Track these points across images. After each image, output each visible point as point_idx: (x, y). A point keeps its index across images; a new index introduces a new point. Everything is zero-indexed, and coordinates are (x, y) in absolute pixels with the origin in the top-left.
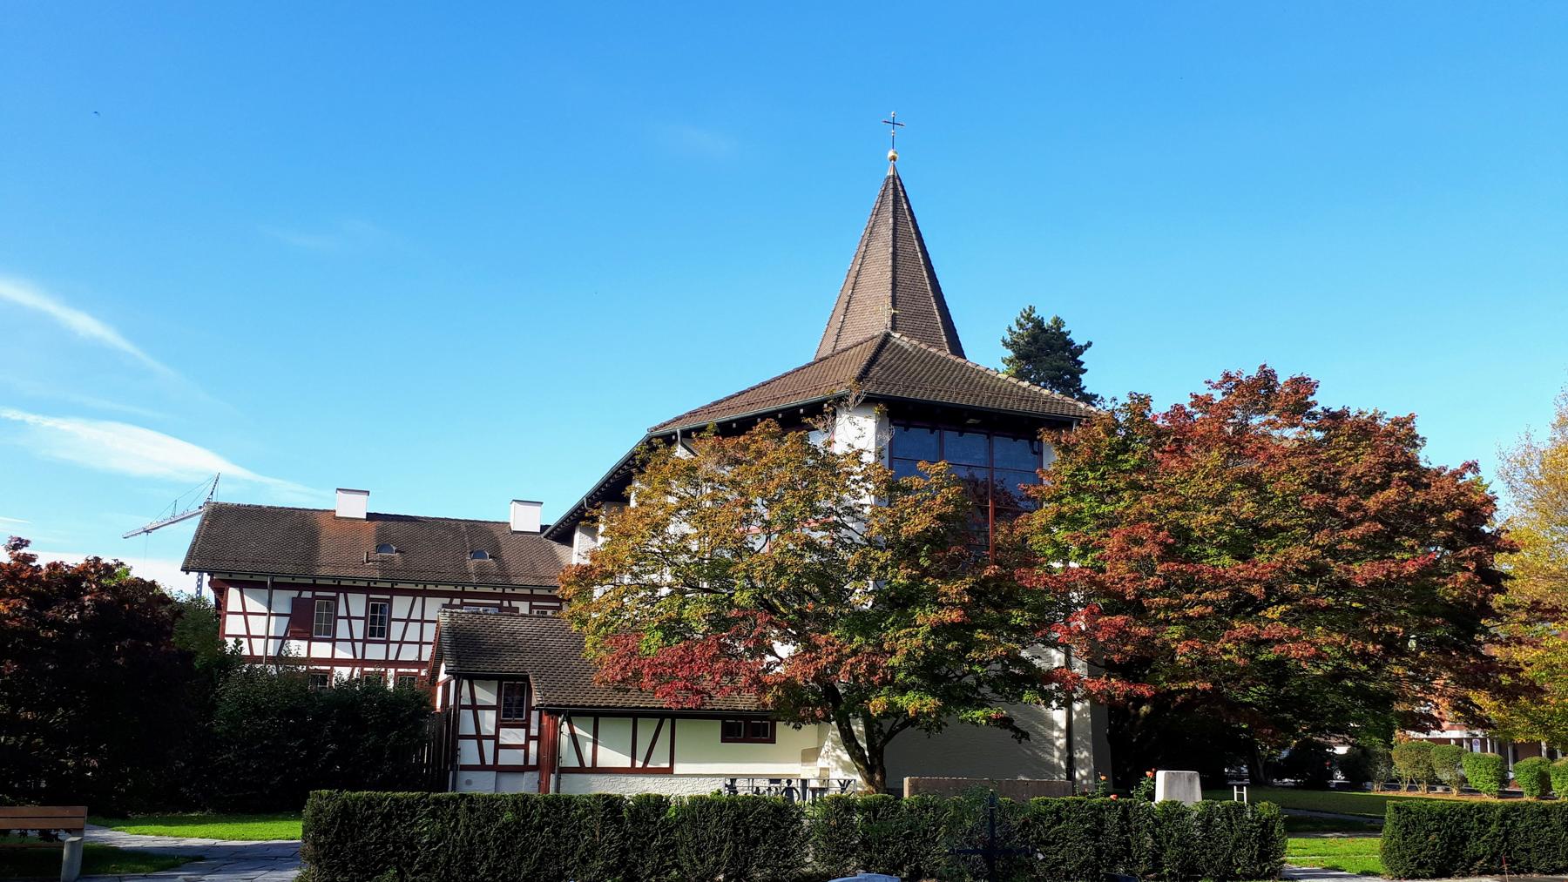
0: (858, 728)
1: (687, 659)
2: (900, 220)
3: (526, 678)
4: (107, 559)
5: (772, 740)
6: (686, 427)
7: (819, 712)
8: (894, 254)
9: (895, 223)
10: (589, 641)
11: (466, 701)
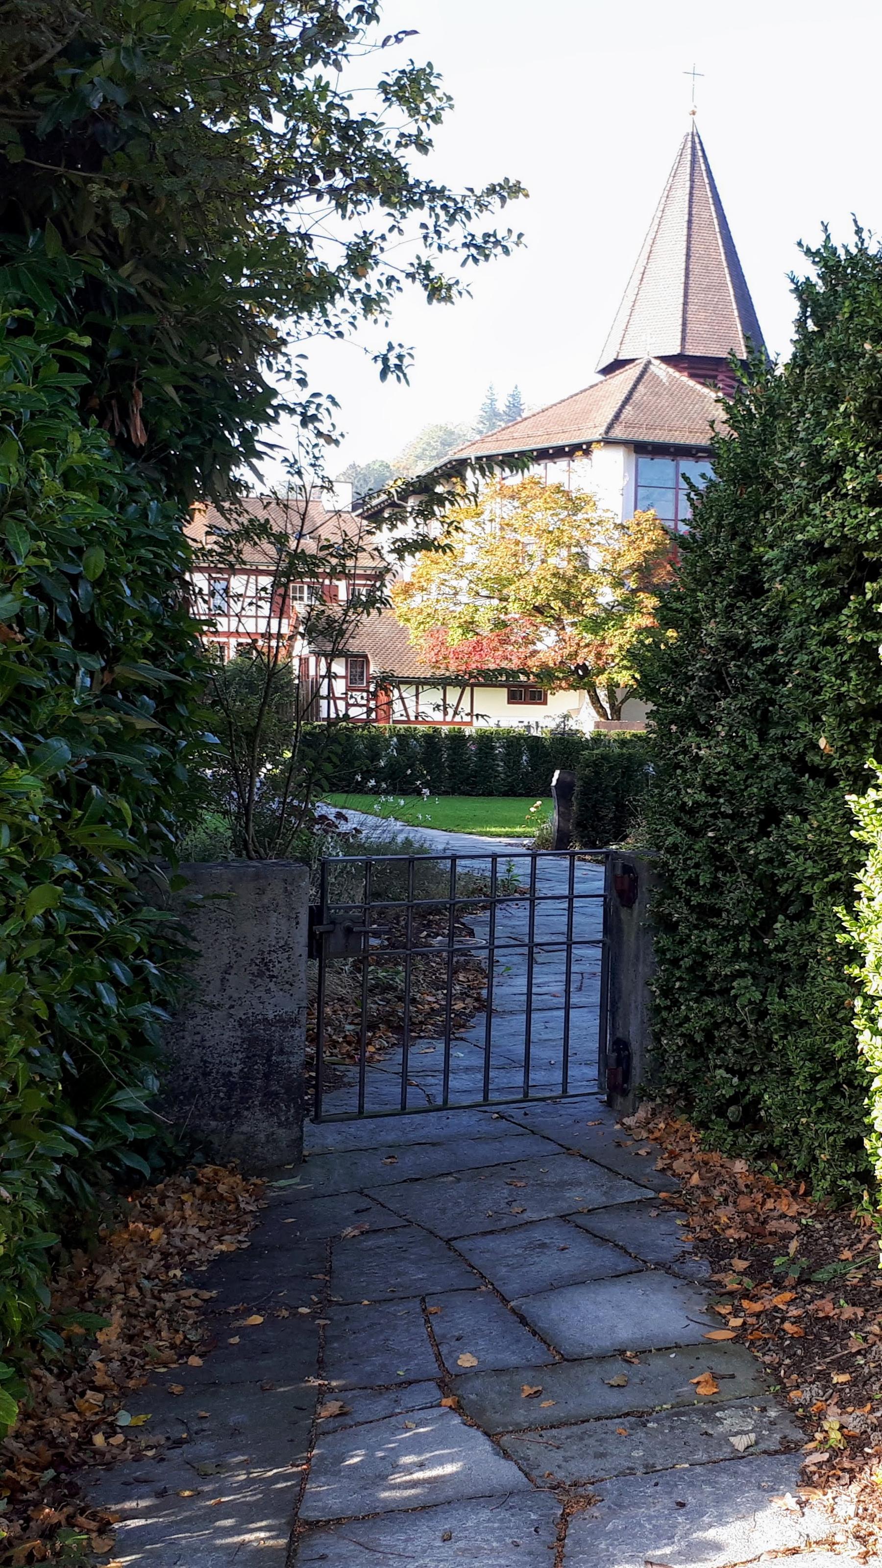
0: (602, 694)
1: (478, 647)
2: (697, 182)
3: (366, 657)
4: (868, 881)
5: (545, 703)
6: (479, 454)
7: (564, 684)
8: (690, 222)
9: (692, 188)
10: (412, 633)
11: (323, 672)
